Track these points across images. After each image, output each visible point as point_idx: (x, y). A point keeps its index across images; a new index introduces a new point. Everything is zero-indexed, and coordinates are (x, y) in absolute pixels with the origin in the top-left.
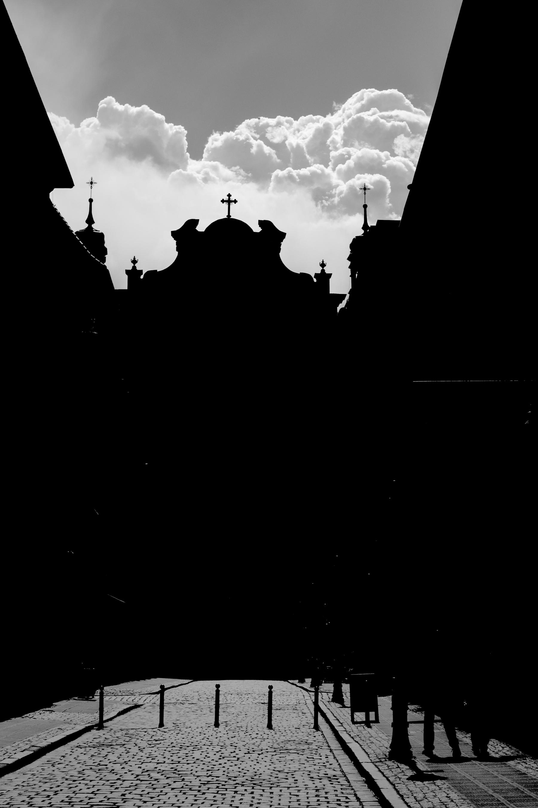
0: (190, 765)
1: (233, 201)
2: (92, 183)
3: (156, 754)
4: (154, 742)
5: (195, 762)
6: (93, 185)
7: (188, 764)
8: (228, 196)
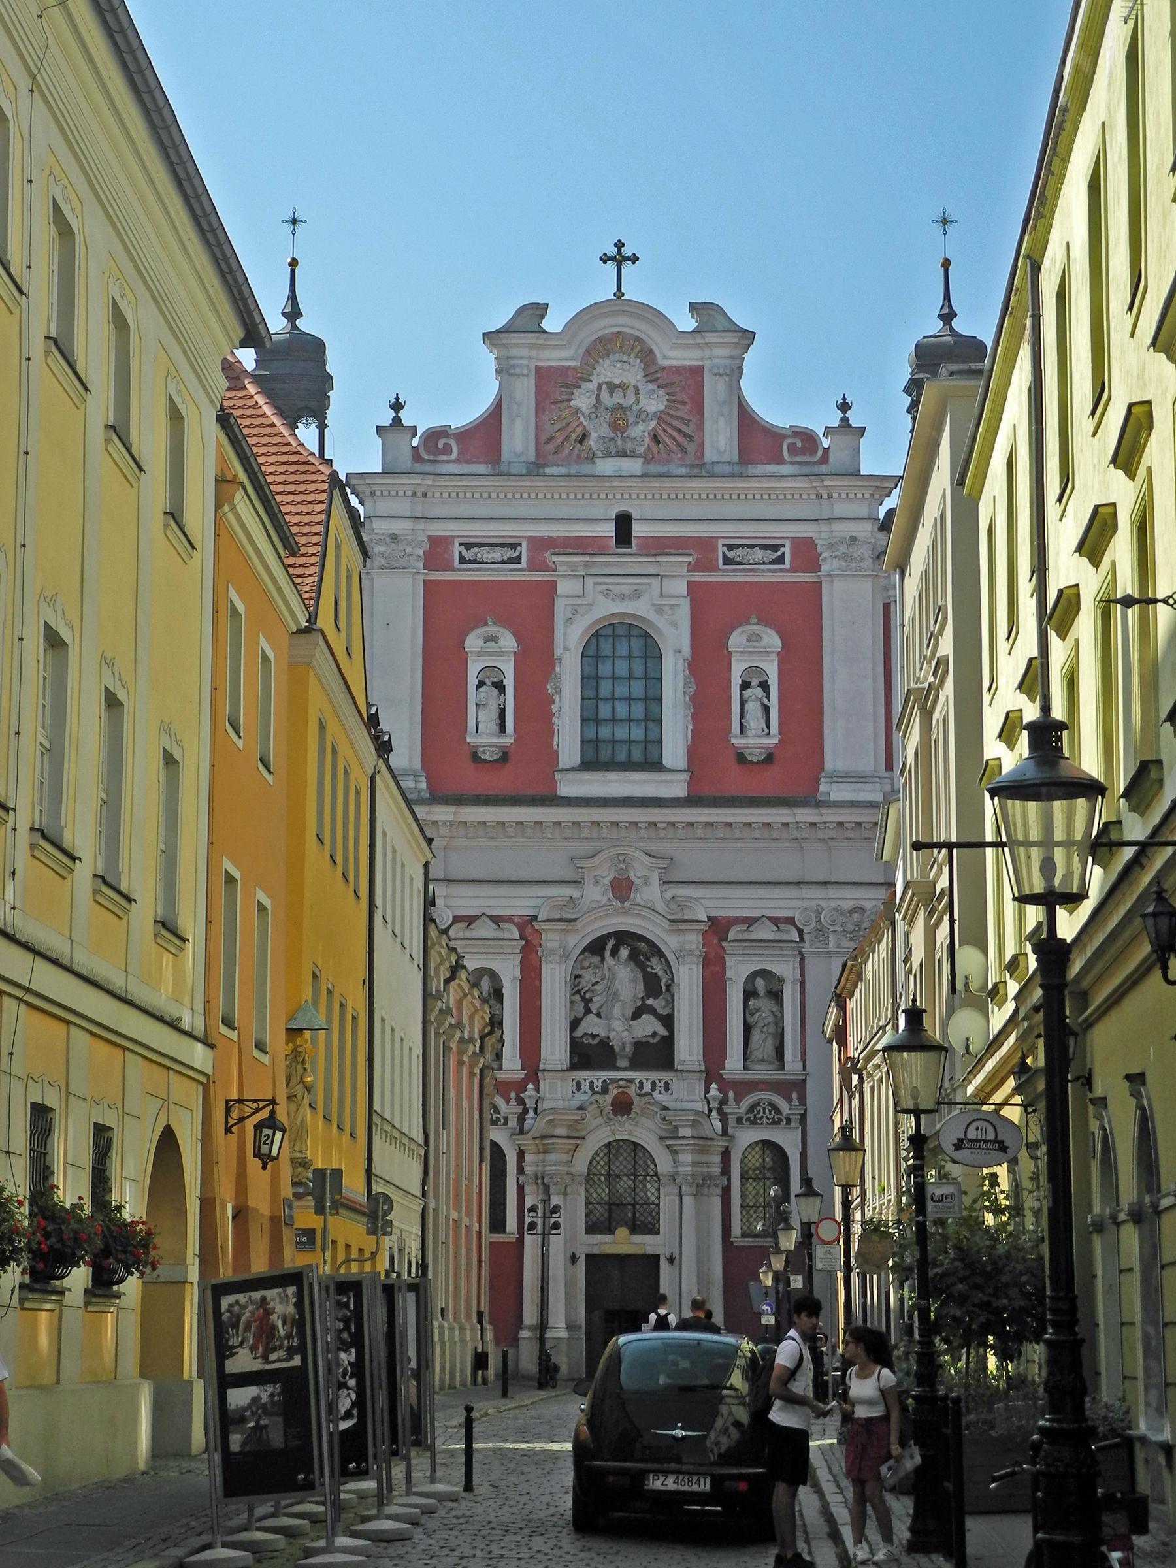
0: (523, 1561)
1: (628, 259)
2: (294, 221)
3: (457, 1542)
4: (455, 1521)
5: (532, 1557)
6: (300, 228)
7: (520, 1559)
8: (616, 245)
